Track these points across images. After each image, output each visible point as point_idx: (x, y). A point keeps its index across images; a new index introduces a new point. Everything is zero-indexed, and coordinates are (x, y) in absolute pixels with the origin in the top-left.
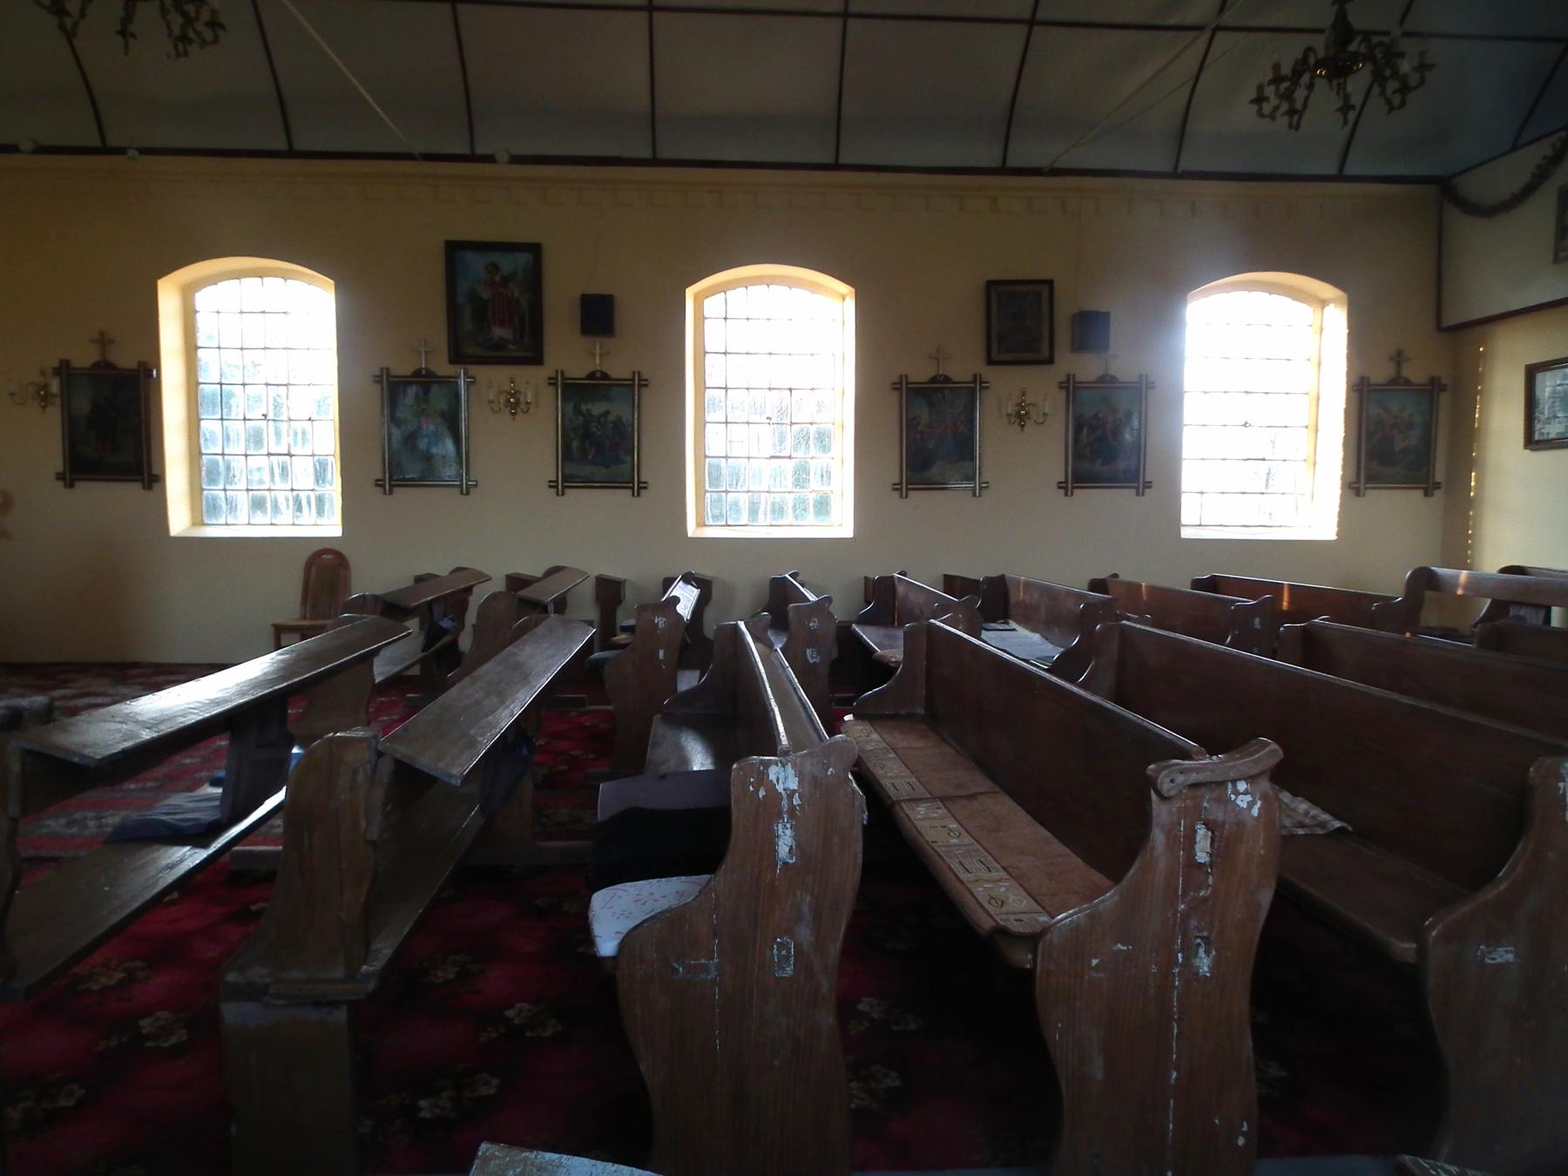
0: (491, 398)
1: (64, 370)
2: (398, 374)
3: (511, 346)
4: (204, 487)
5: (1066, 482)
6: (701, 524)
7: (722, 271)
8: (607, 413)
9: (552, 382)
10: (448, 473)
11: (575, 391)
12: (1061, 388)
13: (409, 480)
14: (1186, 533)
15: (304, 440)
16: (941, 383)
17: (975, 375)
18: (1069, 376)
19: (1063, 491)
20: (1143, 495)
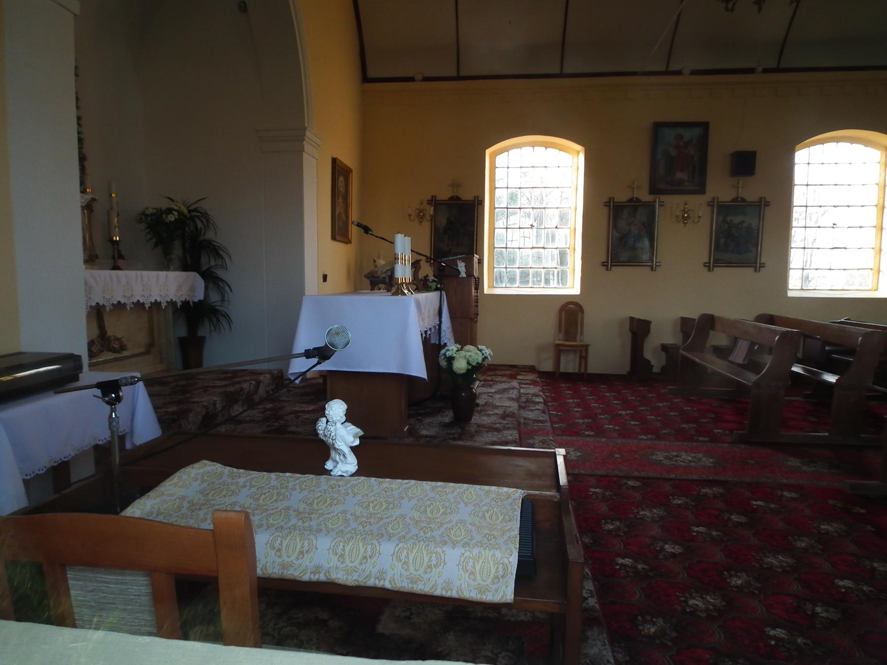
0: (677, 214)
1: (434, 201)
2: (442, 199)
3: (686, 183)
4: (495, 266)
5: (709, 263)
6: (491, 286)
7: (501, 141)
8: (743, 222)
9: (711, 204)
10: (644, 258)
11: (723, 209)
12: (605, 206)
13: (623, 262)
14: (790, 294)
15: (553, 240)
16: (739, 202)
17: (610, 198)
18: (475, 197)
19: (707, 268)
20: (759, 271)
